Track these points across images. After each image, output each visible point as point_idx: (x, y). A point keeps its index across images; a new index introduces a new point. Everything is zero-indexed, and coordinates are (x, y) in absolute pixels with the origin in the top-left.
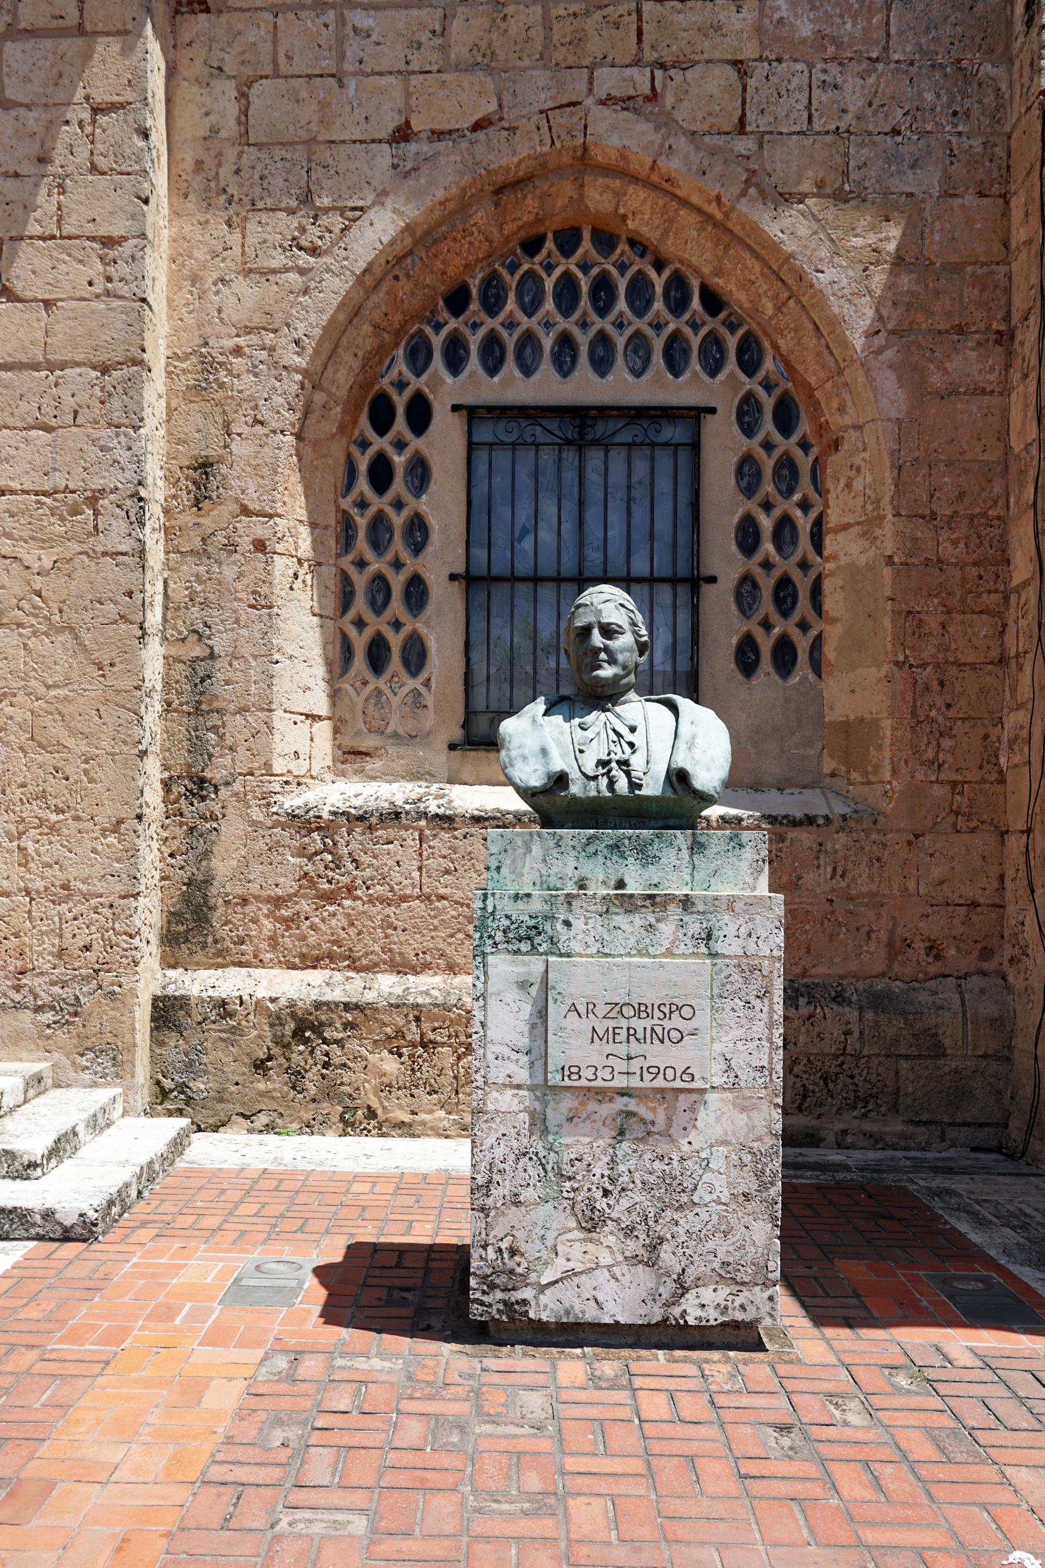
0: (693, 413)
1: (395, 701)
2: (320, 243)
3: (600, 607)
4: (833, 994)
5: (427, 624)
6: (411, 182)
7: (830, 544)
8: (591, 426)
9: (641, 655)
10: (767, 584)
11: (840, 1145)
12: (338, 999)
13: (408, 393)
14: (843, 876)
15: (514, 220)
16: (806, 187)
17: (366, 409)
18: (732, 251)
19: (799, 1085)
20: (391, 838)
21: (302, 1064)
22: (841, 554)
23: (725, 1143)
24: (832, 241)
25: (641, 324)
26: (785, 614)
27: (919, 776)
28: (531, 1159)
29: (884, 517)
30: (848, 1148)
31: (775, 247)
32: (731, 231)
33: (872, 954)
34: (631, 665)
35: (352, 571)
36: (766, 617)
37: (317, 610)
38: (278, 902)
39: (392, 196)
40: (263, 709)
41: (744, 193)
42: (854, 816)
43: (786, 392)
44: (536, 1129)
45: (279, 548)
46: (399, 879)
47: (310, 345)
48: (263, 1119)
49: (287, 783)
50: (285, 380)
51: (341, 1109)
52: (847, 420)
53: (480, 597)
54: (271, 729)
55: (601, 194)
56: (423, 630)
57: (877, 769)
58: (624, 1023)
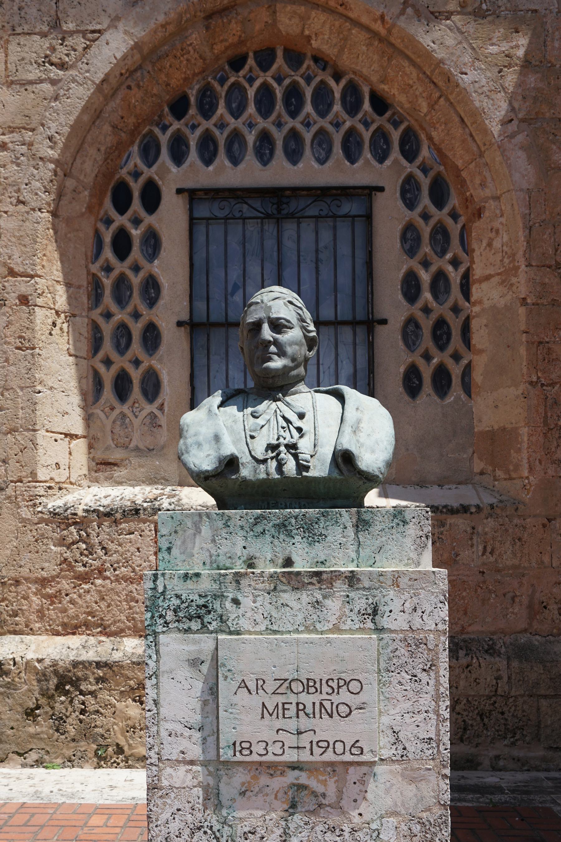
0: (366, 191)
1: (137, 422)
2: (67, 59)
3: (269, 304)
4: (486, 647)
5: (160, 361)
6: (138, 10)
7: (476, 292)
8: (287, 203)
9: (310, 350)
10: (427, 324)
11: (494, 768)
12: (91, 659)
13: (142, 180)
14: (491, 553)
15: (222, 41)
16: (452, 6)
17: (109, 194)
18: (394, 62)
19: (460, 721)
20: (132, 530)
21: (64, 711)
22: (485, 299)
23: (395, 814)
24: (473, 49)
25: (325, 123)
26: (442, 348)
27: (551, 472)
28: (205, 833)
29: (519, 267)
30: (500, 770)
31: (428, 55)
32: (392, 45)
33: (516, 614)
34: (301, 359)
35: (101, 321)
36: (427, 350)
37: (72, 352)
38: (43, 582)
39: (123, 21)
40: (28, 430)
41: (403, 12)
42: (500, 505)
43: (439, 174)
44: (210, 804)
45: (40, 301)
46: (139, 562)
47: (60, 140)
48: (33, 756)
49: (50, 488)
50: (41, 169)
51: (95, 747)
52: (488, 192)
53: (202, 340)
54: (35, 445)
55: (290, 19)
56: (157, 366)
57: (517, 467)
58: (293, 699)
